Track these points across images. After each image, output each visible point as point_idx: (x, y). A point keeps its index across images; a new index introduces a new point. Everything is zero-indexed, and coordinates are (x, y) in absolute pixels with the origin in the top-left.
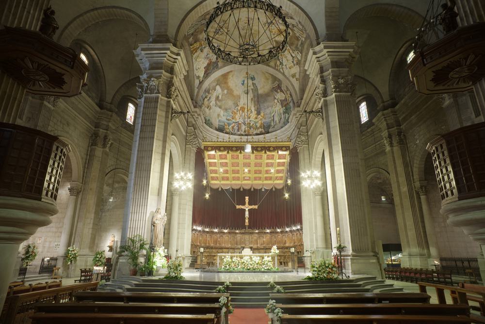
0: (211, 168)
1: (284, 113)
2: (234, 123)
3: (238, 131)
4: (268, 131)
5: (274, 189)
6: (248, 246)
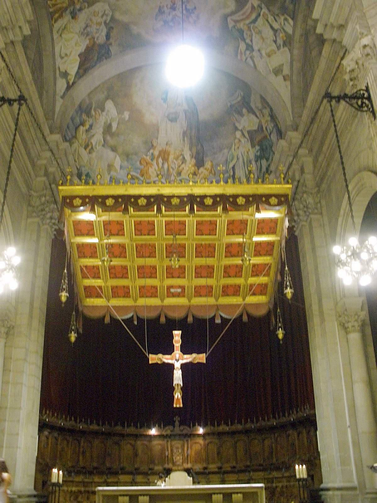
0: (89, 282)
1: (258, 158)
5: (245, 318)
6: (182, 468)
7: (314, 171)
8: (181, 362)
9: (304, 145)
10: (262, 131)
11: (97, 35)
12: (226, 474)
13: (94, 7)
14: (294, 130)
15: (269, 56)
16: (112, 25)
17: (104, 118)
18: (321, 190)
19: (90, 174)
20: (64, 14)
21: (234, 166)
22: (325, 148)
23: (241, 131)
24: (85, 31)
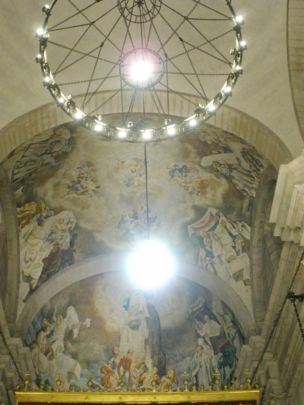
1: (221, 365)
7: (280, 375)
9: (268, 349)
10: (225, 337)
11: (62, 241)
12: (250, 287)
13: (59, 215)
14: (257, 335)
15: (229, 261)
16: (76, 232)
17: (65, 324)
18: (289, 395)
19: (49, 381)
20: (31, 220)
22: (290, 351)
23: (203, 337)
24: (50, 238)
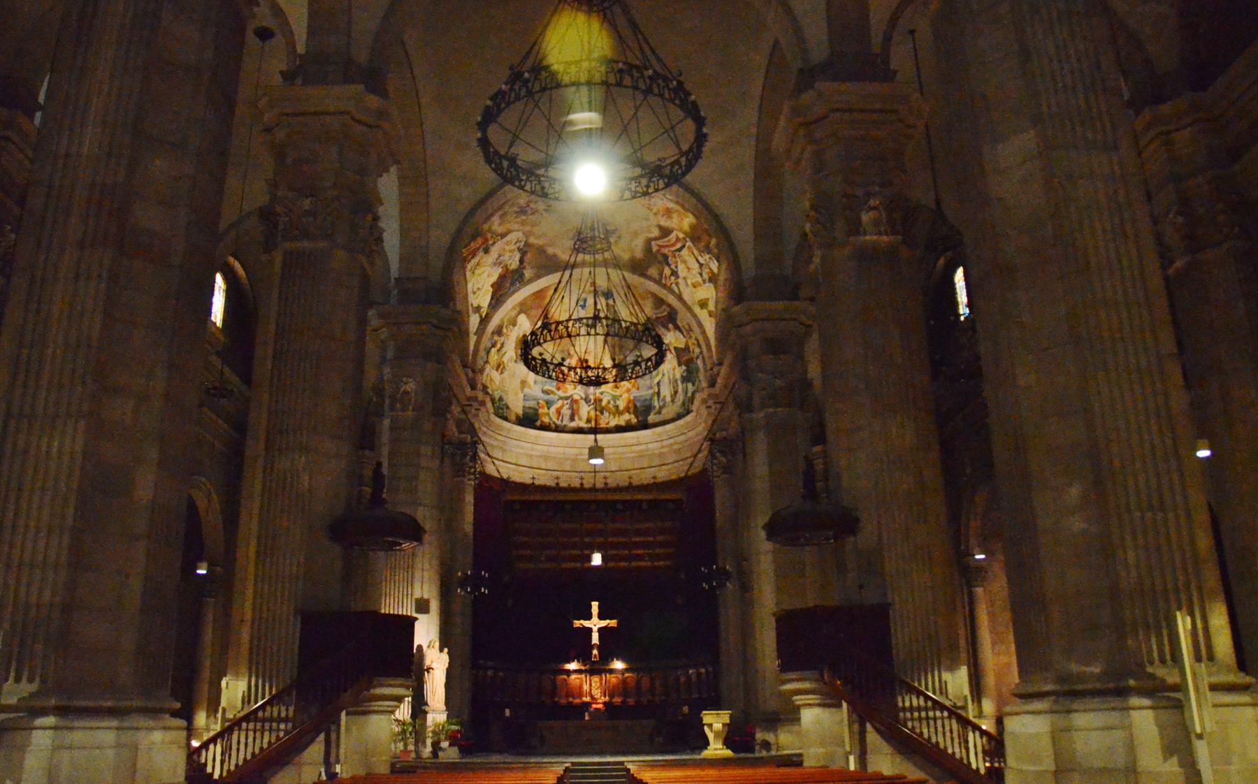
2: (561, 398)
3: (572, 419)
4: (646, 420)
8: (598, 626)
21: (660, 381)
